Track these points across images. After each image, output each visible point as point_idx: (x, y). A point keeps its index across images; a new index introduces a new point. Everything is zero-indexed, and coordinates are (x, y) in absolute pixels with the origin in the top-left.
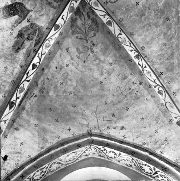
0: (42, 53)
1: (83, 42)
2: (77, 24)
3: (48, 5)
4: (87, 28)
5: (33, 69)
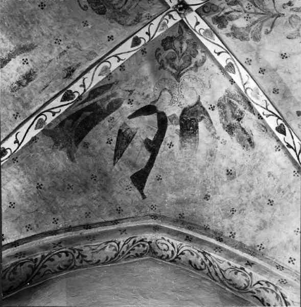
0: (265, 108)
1: (280, 22)
2: (243, 28)
3: (199, 69)
4: (255, 10)
5: (284, 133)
